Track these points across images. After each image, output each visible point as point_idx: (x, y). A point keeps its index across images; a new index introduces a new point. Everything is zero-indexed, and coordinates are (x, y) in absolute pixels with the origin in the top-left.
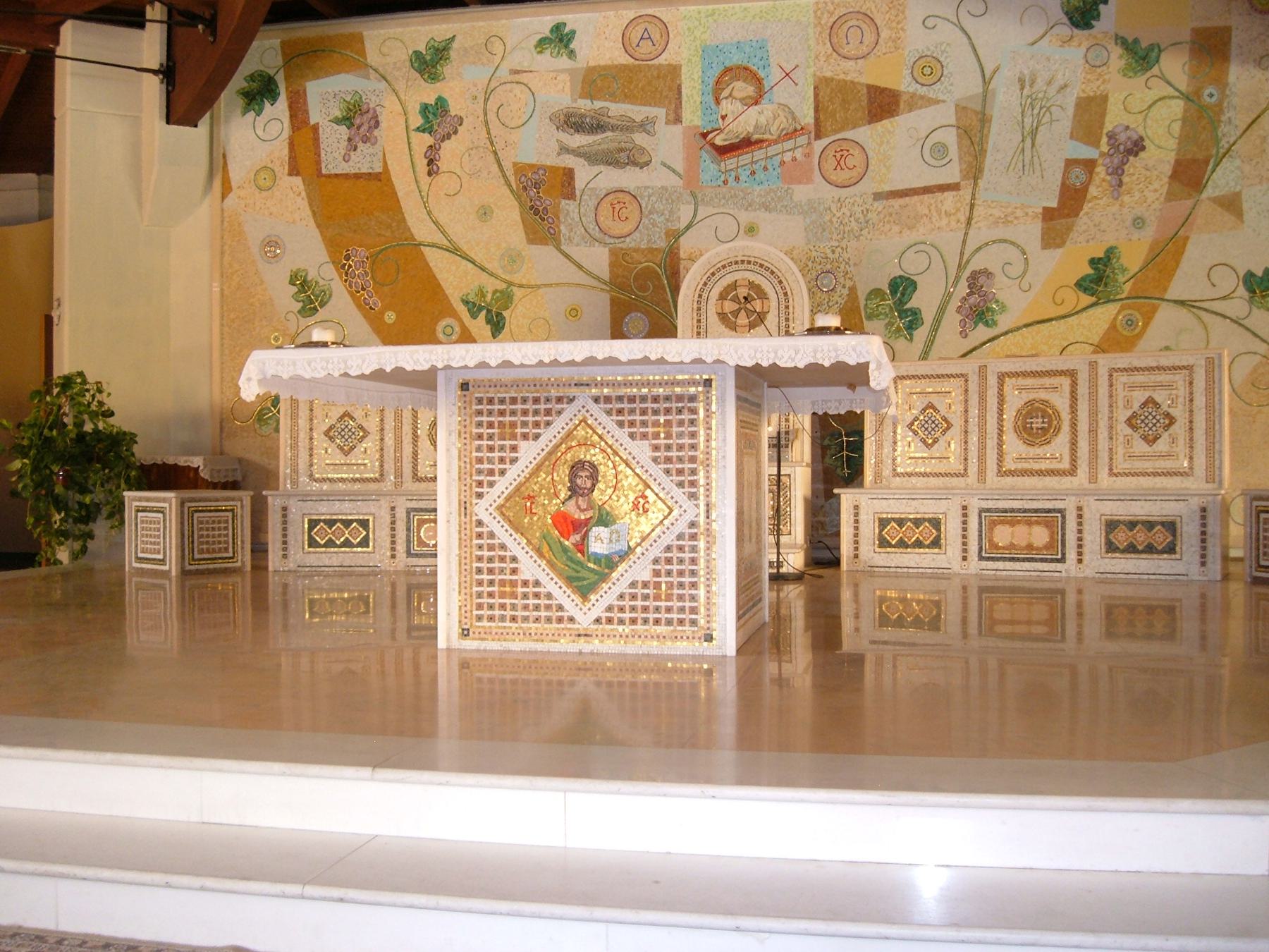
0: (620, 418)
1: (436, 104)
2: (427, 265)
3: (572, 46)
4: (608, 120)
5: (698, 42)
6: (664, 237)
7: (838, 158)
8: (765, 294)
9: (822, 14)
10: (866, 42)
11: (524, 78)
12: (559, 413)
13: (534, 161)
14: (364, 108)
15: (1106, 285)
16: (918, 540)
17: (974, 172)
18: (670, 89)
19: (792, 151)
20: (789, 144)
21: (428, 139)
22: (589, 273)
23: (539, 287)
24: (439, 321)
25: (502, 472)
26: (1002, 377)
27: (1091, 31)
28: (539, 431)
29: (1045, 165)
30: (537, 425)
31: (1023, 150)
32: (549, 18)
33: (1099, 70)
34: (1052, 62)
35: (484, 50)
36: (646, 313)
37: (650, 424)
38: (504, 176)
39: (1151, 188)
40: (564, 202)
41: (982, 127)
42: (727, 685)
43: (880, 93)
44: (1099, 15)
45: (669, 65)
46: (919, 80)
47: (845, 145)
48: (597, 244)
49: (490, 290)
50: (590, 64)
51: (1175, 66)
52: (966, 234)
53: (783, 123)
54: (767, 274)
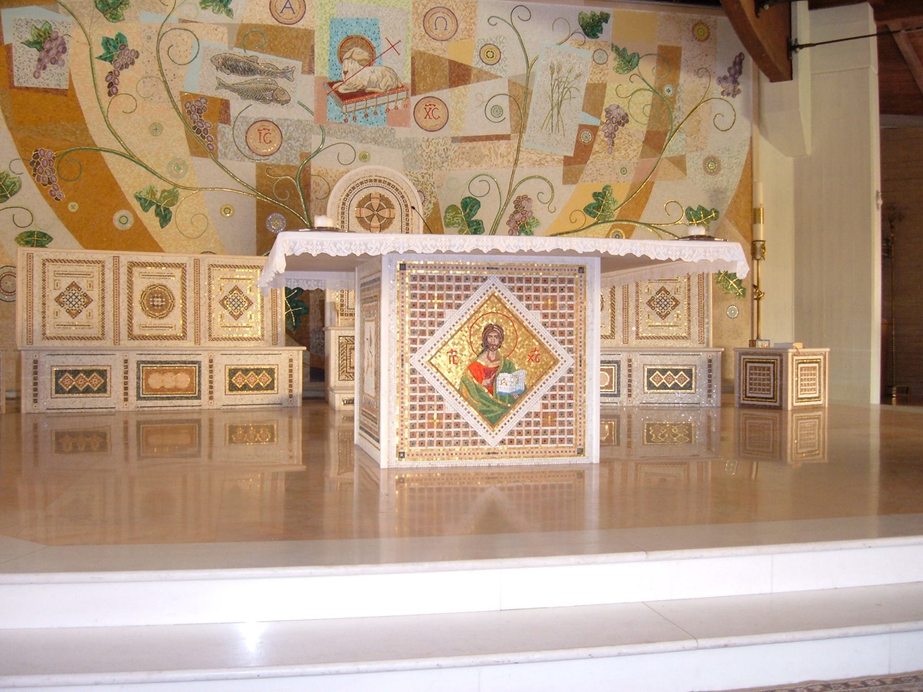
0: (520, 294)
1: (117, 39)
2: (106, 166)
3: (230, 6)
4: (257, 66)
5: (328, 15)
7: (428, 110)
8: (392, 205)
9: (419, 5)
10: (449, 29)
12: (476, 289)
13: (197, 92)
14: (54, 35)
16: (74, 387)
17: (520, 127)
19: (395, 102)
20: (393, 97)
21: (109, 67)
25: (432, 333)
27: (598, 40)
28: (460, 302)
30: (458, 297)
31: (552, 116)
33: (601, 66)
37: (541, 299)
38: (173, 101)
39: (632, 148)
40: (221, 126)
41: (526, 98)
42: (593, 483)
44: (602, 29)
48: (246, 159)
50: (244, 22)
51: (647, 69)
52: (513, 172)
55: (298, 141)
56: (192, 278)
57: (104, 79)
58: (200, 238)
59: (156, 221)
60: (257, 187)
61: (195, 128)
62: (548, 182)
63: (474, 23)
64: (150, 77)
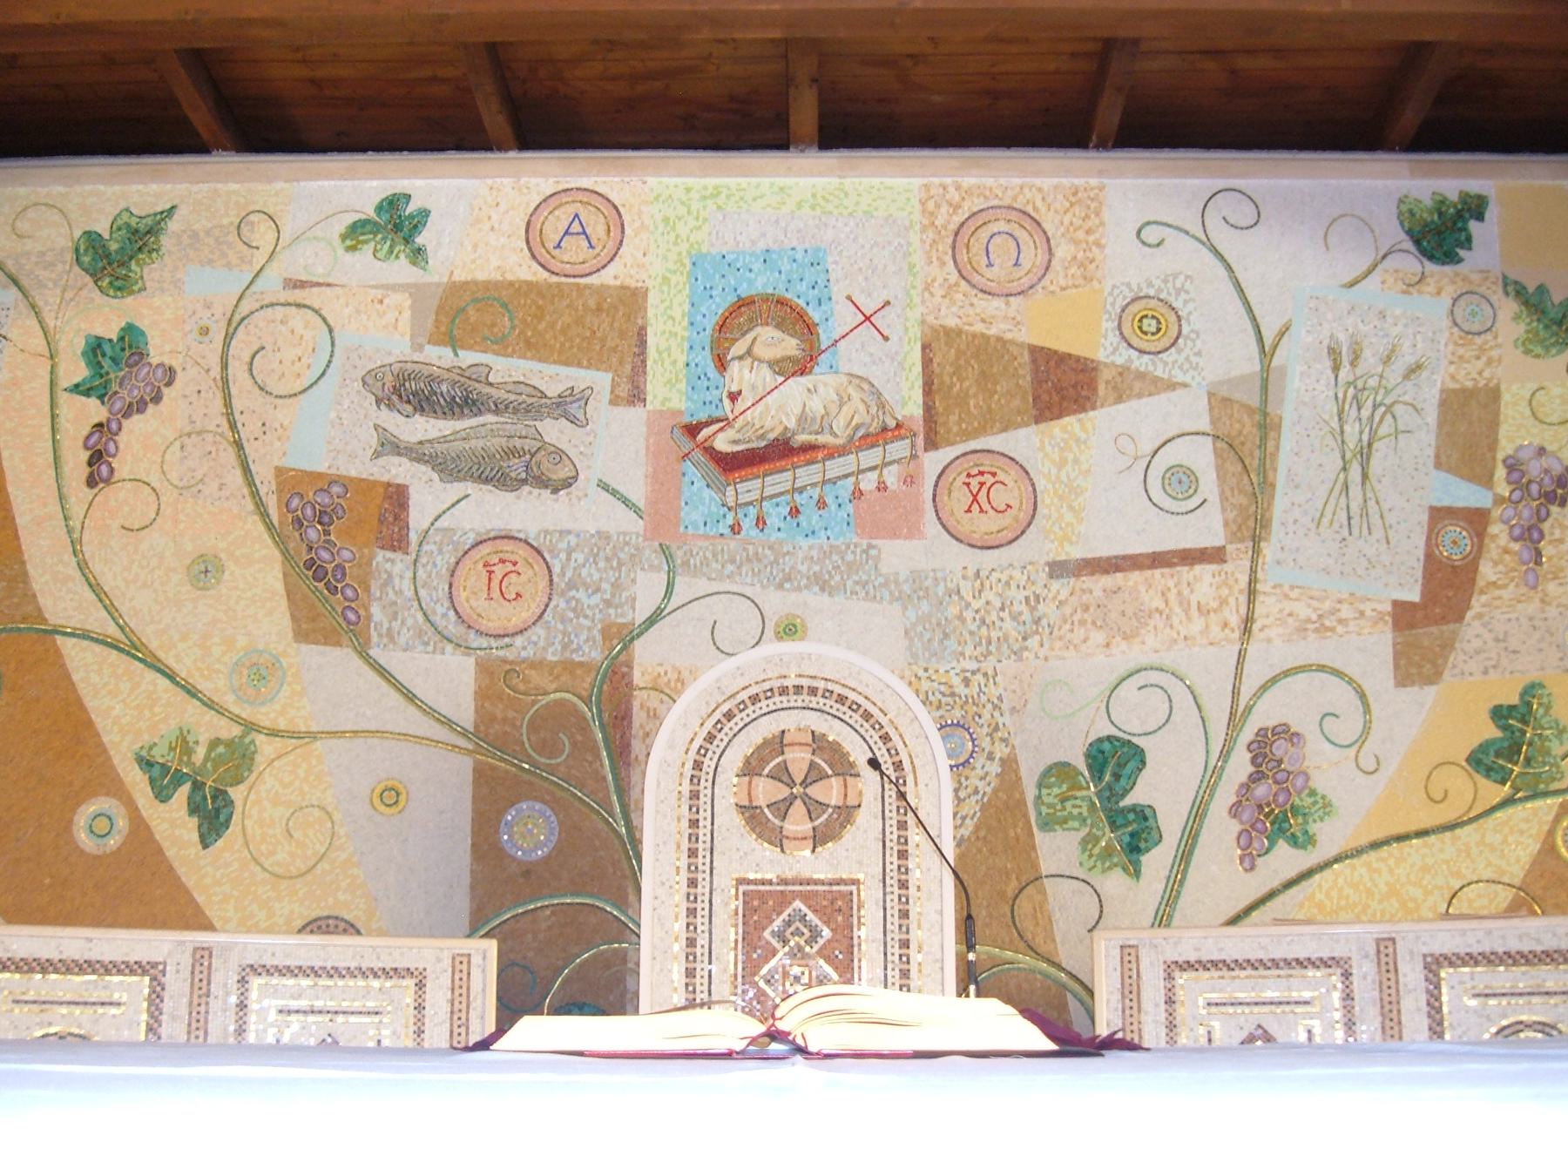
1: (122, 339)
2: (67, 676)
3: (420, 240)
4: (487, 390)
5: (684, 247)
6: (599, 638)
9: (938, 206)
10: (1026, 263)
11: (312, 296)
13: (322, 467)
15: (1528, 761)
18: (622, 335)
20: (871, 457)
21: (95, 410)
22: (430, 712)
23: (313, 736)
24: (78, 805)
26: (1434, 965)
27: (1458, 268)
29: (1391, 518)
31: (1346, 486)
32: (375, 183)
33: (1479, 340)
34: (1389, 320)
35: (233, 237)
36: (555, 803)
38: (255, 494)
40: (381, 556)
41: (1264, 439)
43: (1058, 365)
44: (1469, 239)
45: (623, 287)
46: (1135, 342)
47: (987, 463)
48: (449, 648)
49: (204, 737)
53: (855, 414)
54: (855, 719)
55: (598, 590)
56: (183, 1011)
57: (81, 443)
58: (309, 877)
59: (189, 828)
60: (476, 726)
61: (310, 564)
62: (1351, 681)
63: (1098, 244)
64: (199, 433)
